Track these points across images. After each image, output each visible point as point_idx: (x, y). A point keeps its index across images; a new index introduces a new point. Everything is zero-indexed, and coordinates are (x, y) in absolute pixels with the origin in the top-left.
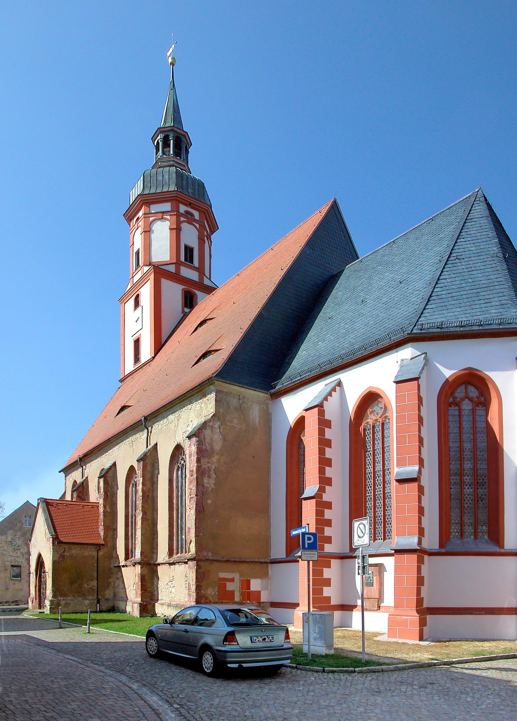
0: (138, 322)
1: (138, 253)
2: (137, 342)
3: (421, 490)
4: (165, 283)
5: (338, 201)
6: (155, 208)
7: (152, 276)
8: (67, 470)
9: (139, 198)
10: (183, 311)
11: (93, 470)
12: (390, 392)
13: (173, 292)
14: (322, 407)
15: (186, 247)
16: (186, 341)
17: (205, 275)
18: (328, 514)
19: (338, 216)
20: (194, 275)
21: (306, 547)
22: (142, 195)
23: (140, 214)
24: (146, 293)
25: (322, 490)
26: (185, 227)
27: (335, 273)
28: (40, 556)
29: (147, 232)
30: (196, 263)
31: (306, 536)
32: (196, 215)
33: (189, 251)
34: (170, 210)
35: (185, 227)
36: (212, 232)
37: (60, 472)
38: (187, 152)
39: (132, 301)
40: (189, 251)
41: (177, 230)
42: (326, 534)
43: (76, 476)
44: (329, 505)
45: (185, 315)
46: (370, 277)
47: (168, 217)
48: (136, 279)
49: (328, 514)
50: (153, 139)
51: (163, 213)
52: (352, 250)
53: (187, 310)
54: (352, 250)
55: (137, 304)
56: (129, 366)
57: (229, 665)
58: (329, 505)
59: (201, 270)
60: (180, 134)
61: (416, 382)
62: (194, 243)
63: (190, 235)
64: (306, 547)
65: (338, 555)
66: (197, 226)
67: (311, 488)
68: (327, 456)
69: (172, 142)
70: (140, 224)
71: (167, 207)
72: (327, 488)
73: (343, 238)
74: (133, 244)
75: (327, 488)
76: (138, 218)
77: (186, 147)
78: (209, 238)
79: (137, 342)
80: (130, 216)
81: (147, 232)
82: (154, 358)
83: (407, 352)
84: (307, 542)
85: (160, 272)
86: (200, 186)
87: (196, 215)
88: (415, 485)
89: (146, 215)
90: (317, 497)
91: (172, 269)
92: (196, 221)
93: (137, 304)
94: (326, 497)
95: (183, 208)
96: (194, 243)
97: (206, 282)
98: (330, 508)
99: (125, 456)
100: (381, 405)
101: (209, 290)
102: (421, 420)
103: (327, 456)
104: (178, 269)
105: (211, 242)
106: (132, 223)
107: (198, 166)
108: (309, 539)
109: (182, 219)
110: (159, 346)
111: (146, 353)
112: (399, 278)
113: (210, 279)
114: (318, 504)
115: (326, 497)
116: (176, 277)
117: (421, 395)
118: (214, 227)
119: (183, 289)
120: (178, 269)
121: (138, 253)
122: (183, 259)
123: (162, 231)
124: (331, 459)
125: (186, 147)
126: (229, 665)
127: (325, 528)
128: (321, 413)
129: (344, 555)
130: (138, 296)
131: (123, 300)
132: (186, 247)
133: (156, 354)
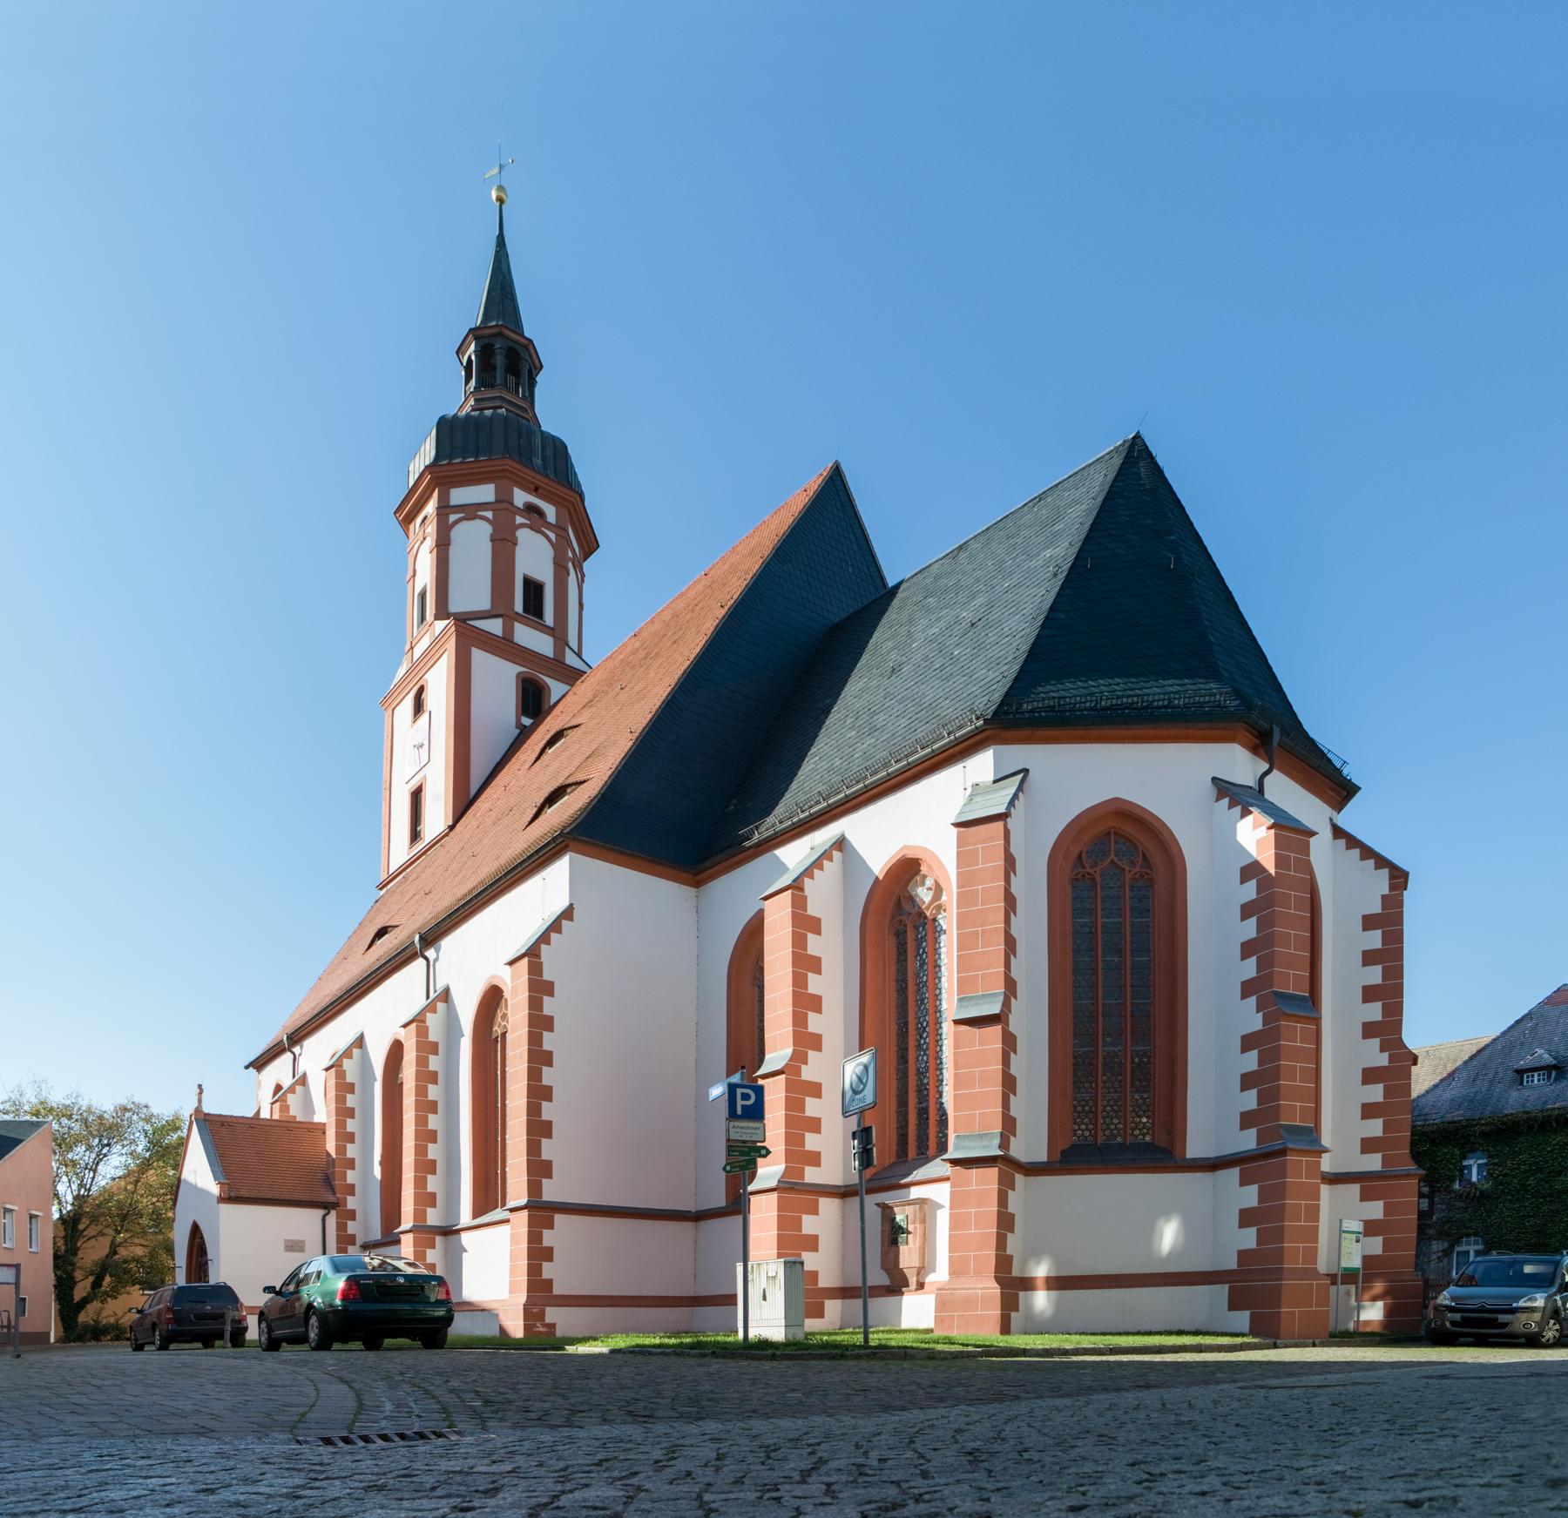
0: (420, 752)
1: (423, 595)
2: (417, 796)
3: (1009, 1042)
4: (479, 657)
5: (844, 468)
6: (460, 496)
7: (451, 644)
8: (259, 1064)
10: (519, 725)
11: (317, 1052)
12: (942, 849)
13: (497, 680)
16: (525, 780)
20: (542, 644)
21: (739, 1112)
23: (430, 508)
24: (439, 683)
25: (799, 1058)
26: (524, 536)
27: (838, 614)
28: (196, 1230)
30: (549, 618)
31: (739, 1091)
32: (550, 512)
33: (533, 590)
35: (524, 536)
36: (587, 556)
37: (247, 1067)
38: (532, 383)
39: (408, 704)
41: (503, 546)
42: (808, 1147)
43: (280, 1071)
45: (524, 734)
46: (911, 621)
47: (489, 514)
48: (418, 651)
50: (460, 351)
53: (527, 721)
55: (419, 707)
56: (400, 851)
57: (570, 1349)
59: (558, 633)
60: (516, 342)
61: (1000, 824)
62: (544, 573)
63: (534, 556)
64: (739, 1112)
66: (552, 536)
67: (777, 1054)
68: (812, 989)
71: (485, 493)
72: (811, 1054)
73: (855, 547)
75: (811, 1054)
77: (530, 371)
78: (579, 567)
79: (417, 796)
80: (407, 514)
82: (452, 828)
83: (982, 765)
84: (740, 1103)
85: (468, 634)
87: (550, 512)
88: (996, 1030)
89: (444, 509)
90: (790, 1070)
91: (495, 626)
92: (549, 526)
93: (419, 707)
94: (808, 1073)
95: (521, 497)
96: (544, 573)
97: (571, 659)
99: (383, 1016)
100: (929, 882)
101: (572, 676)
102: (1010, 902)
103: (812, 989)
104: (508, 629)
105: (583, 576)
107: (553, 409)
108: (745, 1097)
109: (519, 520)
110: (464, 802)
111: (436, 817)
112: (967, 615)
113: (579, 655)
114: (790, 1086)
115: (808, 1073)
116: (505, 647)
117: (1013, 850)
118: (589, 544)
119: (518, 675)
120: (508, 629)
121: (423, 595)
122: (519, 607)
123: (474, 539)
124: (820, 998)
125: (530, 371)
126: (570, 1349)
128: (799, 902)
130: (421, 690)
131: (389, 702)
133: (457, 820)
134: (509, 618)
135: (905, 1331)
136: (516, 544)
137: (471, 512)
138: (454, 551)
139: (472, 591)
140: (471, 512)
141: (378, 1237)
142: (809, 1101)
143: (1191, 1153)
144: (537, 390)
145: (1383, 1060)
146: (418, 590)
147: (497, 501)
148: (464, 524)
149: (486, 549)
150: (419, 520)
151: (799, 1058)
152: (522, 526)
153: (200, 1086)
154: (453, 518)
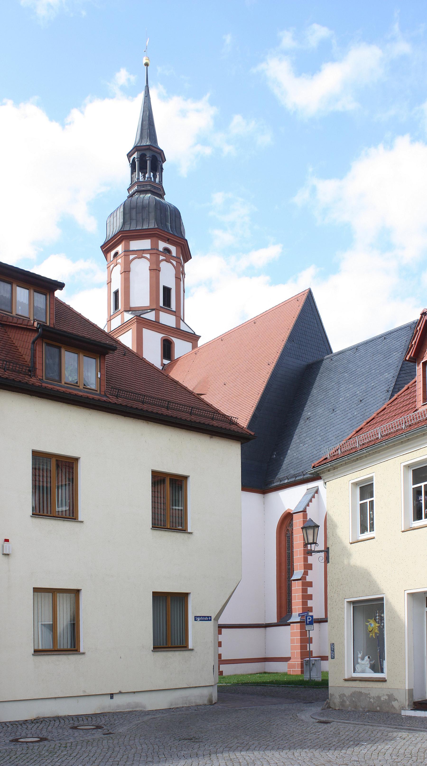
4: (147, 333)
6: (135, 245)
9: (120, 233)
14: (306, 512)
15: (165, 288)
17: (183, 321)
18: (310, 591)
19: (312, 304)
22: (123, 231)
25: (306, 573)
29: (126, 272)
30: (173, 306)
31: (308, 617)
32: (173, 249)
33: (167, 291)
34: (150, 248)
40: (167, 291)
41: (155, 271)
44: (310, 584)
49: (310, 591)
50: (129, 155)
51: (144, 251)
52: (325, 340)
53: (166, 362)
54: (327, 346)
58: (310, 584)
59: (178, 315)
63: (167, 277)
65: (317, 620)
66: (174, 263)
67: (298, 574)
68: (309, 562)
69: (148, 162)
70: (119, 261)
71: (145, 244)
74: (111, 282)
76: (116, 254)
81: (126, 272)
84: (308, 620)
86: (176, 215)
89: (127, 252)
90: (303, 578)
91: (151, 316)
94: (308, 579)
95: (162, 245)
97: (183, 327)
98: (311, 586)
103: (309, 562)
104: (157, 316)
106: (108, 255)
108: (309, 619)
109: (161, 258)
115: (308, 579)
116: (156, 326)
120: (157, 316)
122: (161, 304)
123: (141, 268)
127: (308, 601)
128: (305, 516)
129: (321, 620)
132: (165, 288)
134: (157, 310)
135: (182, 330)
136: (160, 271)
137: (140, 253)
138: (132, 275)
139: (141, 296)
140: (140, 253)
141: (69, 647)
142: (309, 602)
143: (313, 656)
144: (163, 173)
145: (214, 702)
146: (113, 290)
147: (152, 249)
148: (137, 260)
149: (147, 273)
150: (113, 253)
151: (306, 573)
152: (163, 260)
153: (374, 538)
154: (131, 257)
